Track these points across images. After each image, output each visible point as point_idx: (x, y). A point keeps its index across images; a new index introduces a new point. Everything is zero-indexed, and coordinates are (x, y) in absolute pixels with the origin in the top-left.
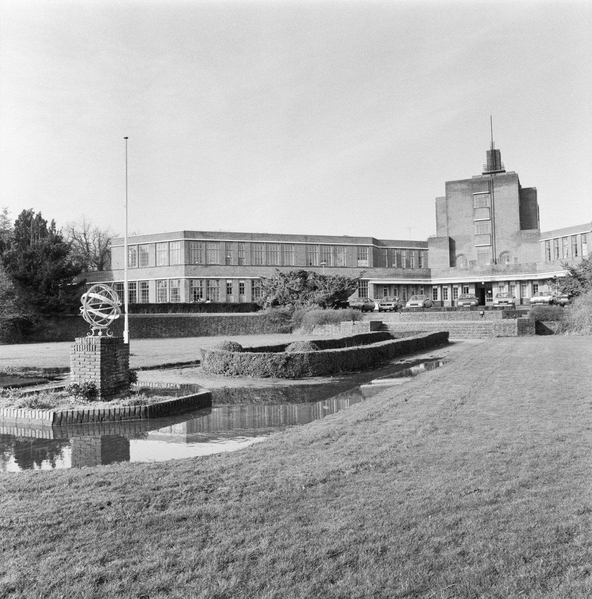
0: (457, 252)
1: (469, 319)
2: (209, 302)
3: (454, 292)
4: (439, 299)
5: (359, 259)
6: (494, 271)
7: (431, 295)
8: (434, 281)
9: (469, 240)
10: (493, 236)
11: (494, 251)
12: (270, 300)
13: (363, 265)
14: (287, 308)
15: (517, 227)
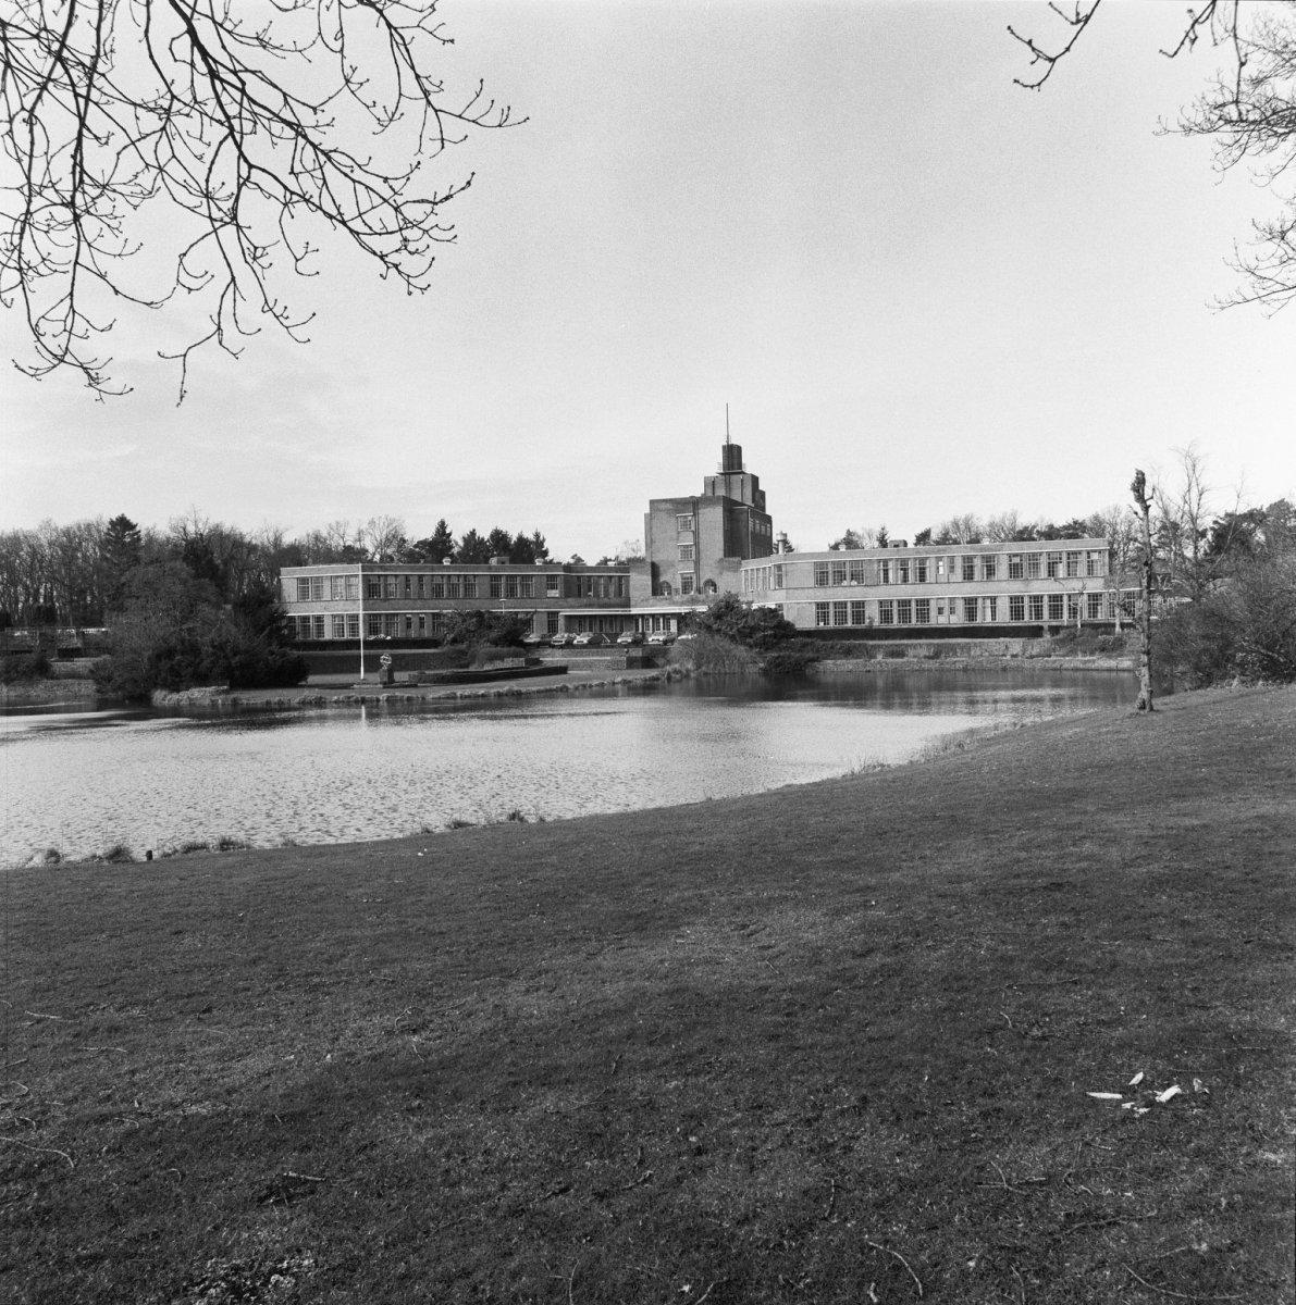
2: (389, 638)
4: (640, 631)
8: (634, 611)
12: (450, 637)
14: (463, 646)
15: (721, 554)
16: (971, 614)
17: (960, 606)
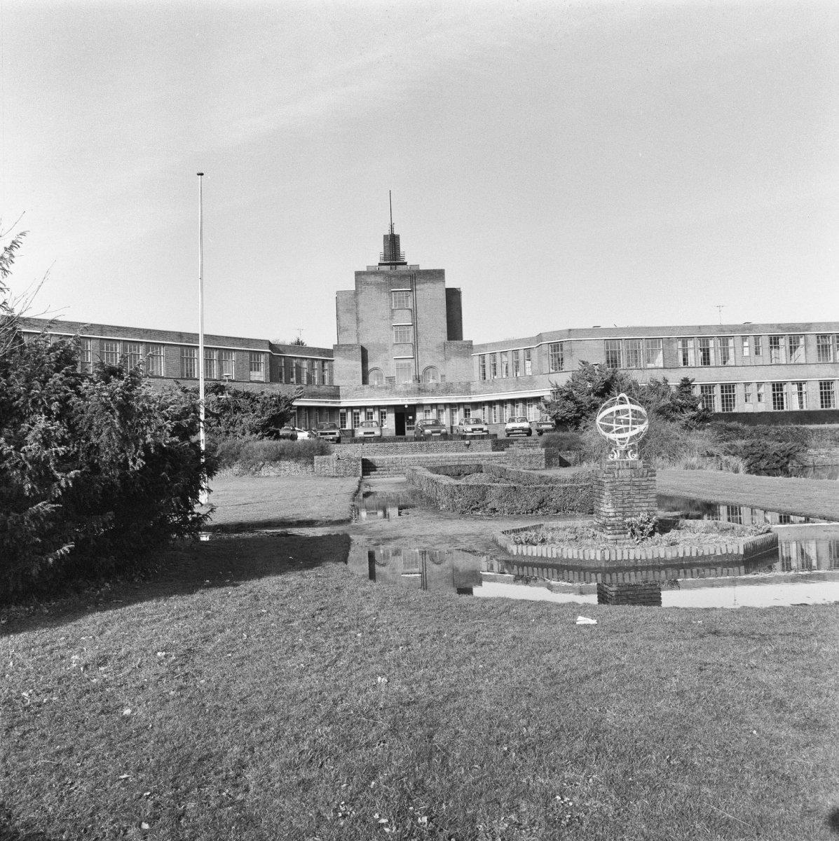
0: (370, 366)
1: (453, 451)
3: (355, 419)
5: (251, 370)
6: (421, 391)
7: (338, 422)
8: (345, 403)
9: (386, 350)
10: (415, 346)
11: (417, 365)
13: (257, 379)
16: (778, 400)
17: (767, 392)
